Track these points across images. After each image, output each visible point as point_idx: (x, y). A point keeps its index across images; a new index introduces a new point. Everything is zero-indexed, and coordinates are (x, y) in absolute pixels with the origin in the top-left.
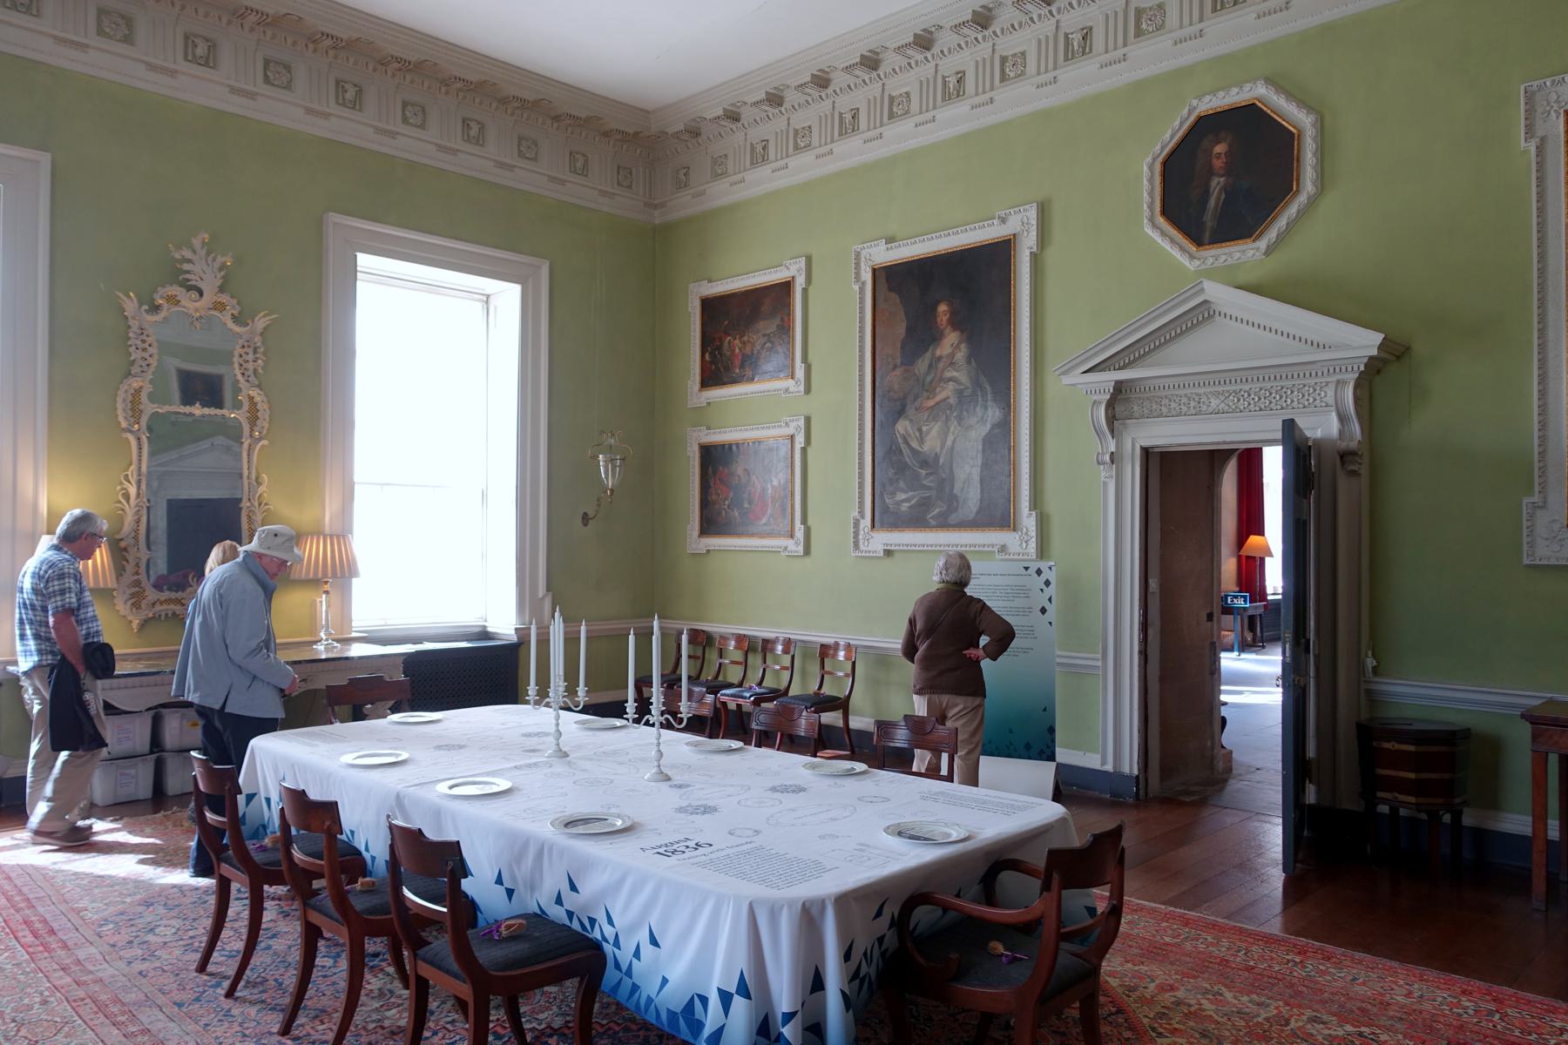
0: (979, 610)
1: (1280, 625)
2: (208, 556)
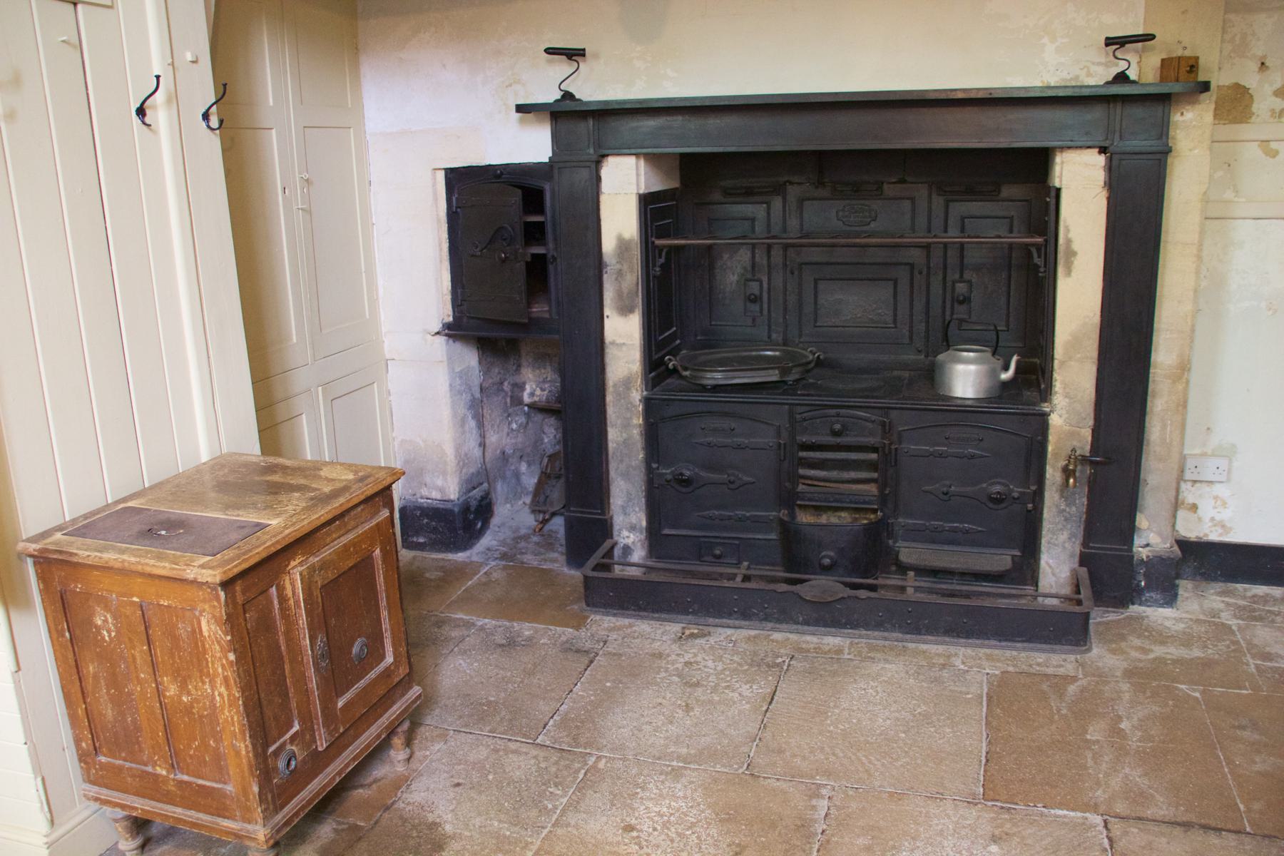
0: (397, 741)
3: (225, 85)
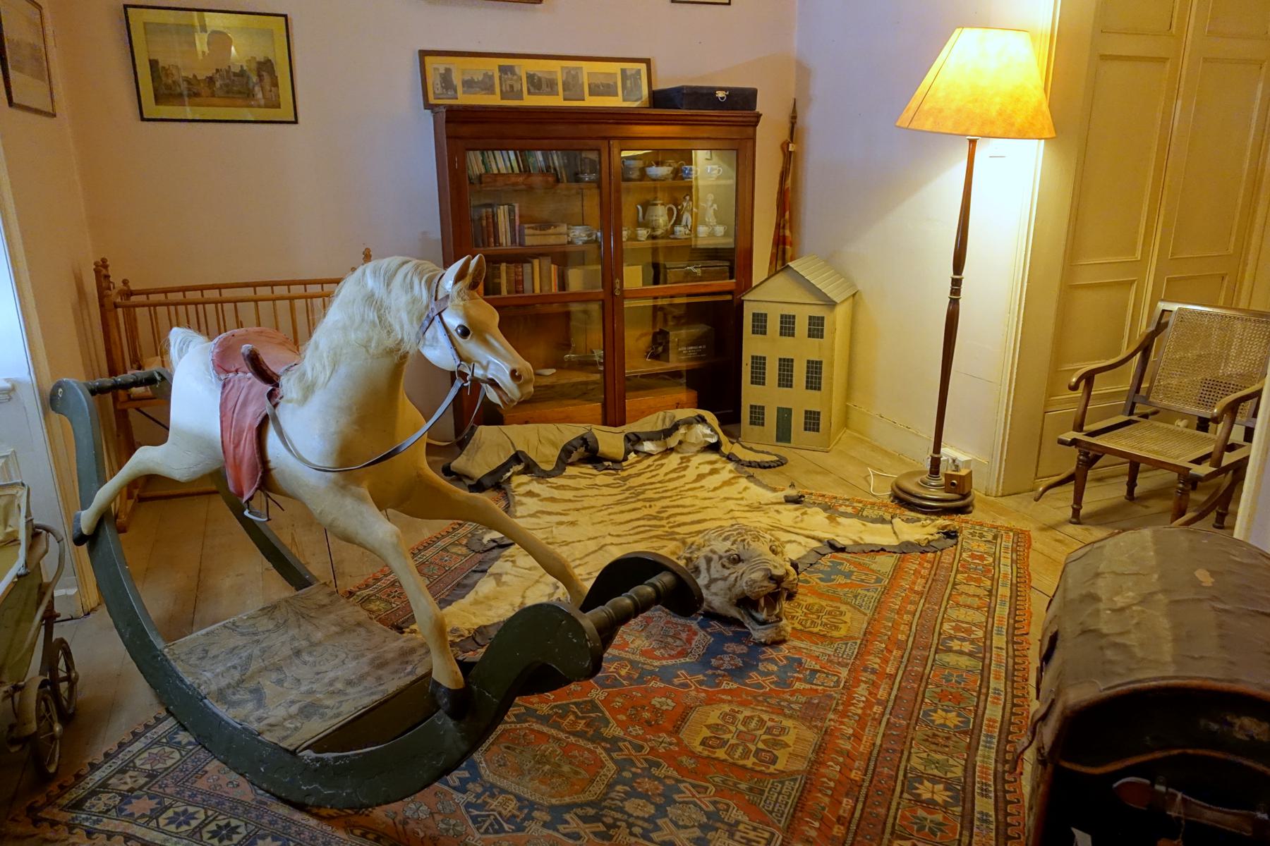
1: (655, 107)
3: (729, 4)
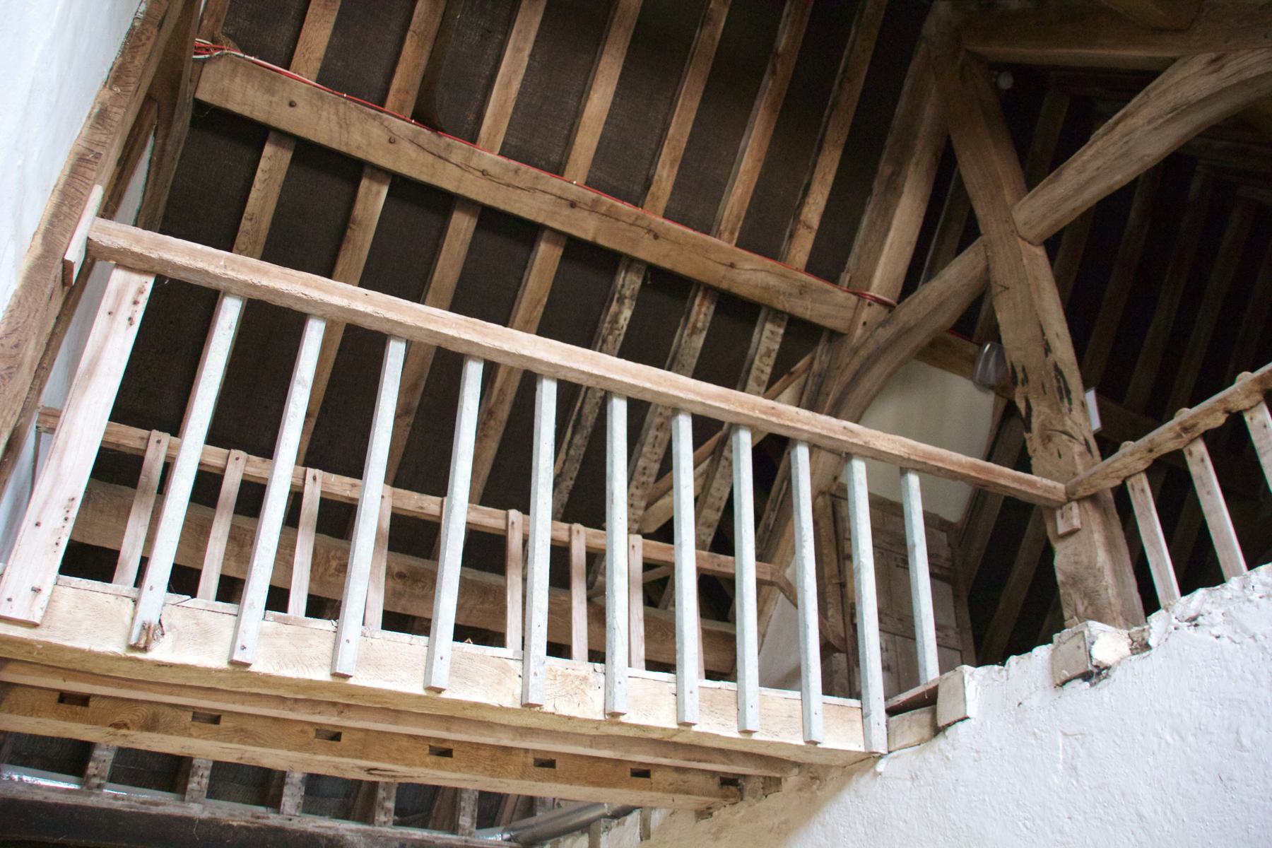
2: (1042, 180)
3: (363, 624)
